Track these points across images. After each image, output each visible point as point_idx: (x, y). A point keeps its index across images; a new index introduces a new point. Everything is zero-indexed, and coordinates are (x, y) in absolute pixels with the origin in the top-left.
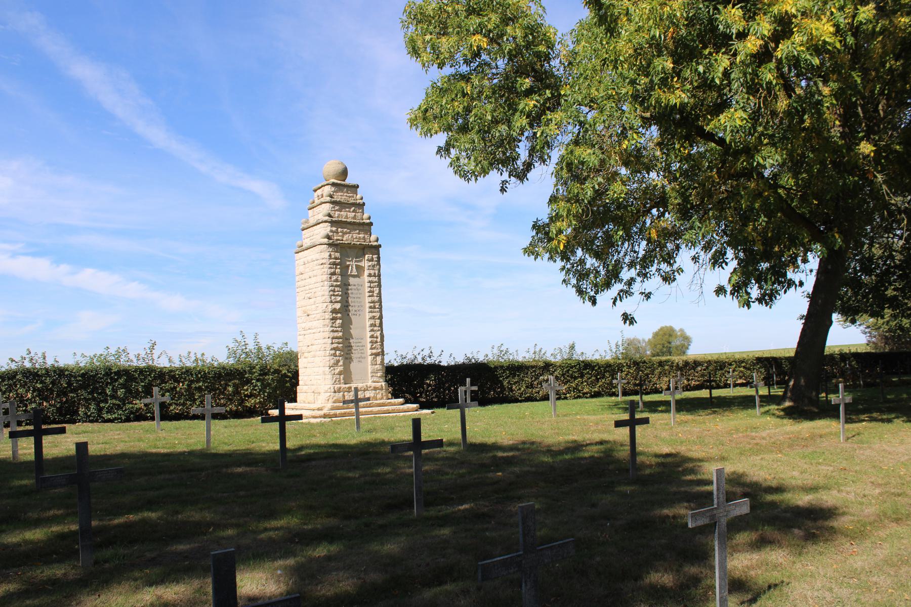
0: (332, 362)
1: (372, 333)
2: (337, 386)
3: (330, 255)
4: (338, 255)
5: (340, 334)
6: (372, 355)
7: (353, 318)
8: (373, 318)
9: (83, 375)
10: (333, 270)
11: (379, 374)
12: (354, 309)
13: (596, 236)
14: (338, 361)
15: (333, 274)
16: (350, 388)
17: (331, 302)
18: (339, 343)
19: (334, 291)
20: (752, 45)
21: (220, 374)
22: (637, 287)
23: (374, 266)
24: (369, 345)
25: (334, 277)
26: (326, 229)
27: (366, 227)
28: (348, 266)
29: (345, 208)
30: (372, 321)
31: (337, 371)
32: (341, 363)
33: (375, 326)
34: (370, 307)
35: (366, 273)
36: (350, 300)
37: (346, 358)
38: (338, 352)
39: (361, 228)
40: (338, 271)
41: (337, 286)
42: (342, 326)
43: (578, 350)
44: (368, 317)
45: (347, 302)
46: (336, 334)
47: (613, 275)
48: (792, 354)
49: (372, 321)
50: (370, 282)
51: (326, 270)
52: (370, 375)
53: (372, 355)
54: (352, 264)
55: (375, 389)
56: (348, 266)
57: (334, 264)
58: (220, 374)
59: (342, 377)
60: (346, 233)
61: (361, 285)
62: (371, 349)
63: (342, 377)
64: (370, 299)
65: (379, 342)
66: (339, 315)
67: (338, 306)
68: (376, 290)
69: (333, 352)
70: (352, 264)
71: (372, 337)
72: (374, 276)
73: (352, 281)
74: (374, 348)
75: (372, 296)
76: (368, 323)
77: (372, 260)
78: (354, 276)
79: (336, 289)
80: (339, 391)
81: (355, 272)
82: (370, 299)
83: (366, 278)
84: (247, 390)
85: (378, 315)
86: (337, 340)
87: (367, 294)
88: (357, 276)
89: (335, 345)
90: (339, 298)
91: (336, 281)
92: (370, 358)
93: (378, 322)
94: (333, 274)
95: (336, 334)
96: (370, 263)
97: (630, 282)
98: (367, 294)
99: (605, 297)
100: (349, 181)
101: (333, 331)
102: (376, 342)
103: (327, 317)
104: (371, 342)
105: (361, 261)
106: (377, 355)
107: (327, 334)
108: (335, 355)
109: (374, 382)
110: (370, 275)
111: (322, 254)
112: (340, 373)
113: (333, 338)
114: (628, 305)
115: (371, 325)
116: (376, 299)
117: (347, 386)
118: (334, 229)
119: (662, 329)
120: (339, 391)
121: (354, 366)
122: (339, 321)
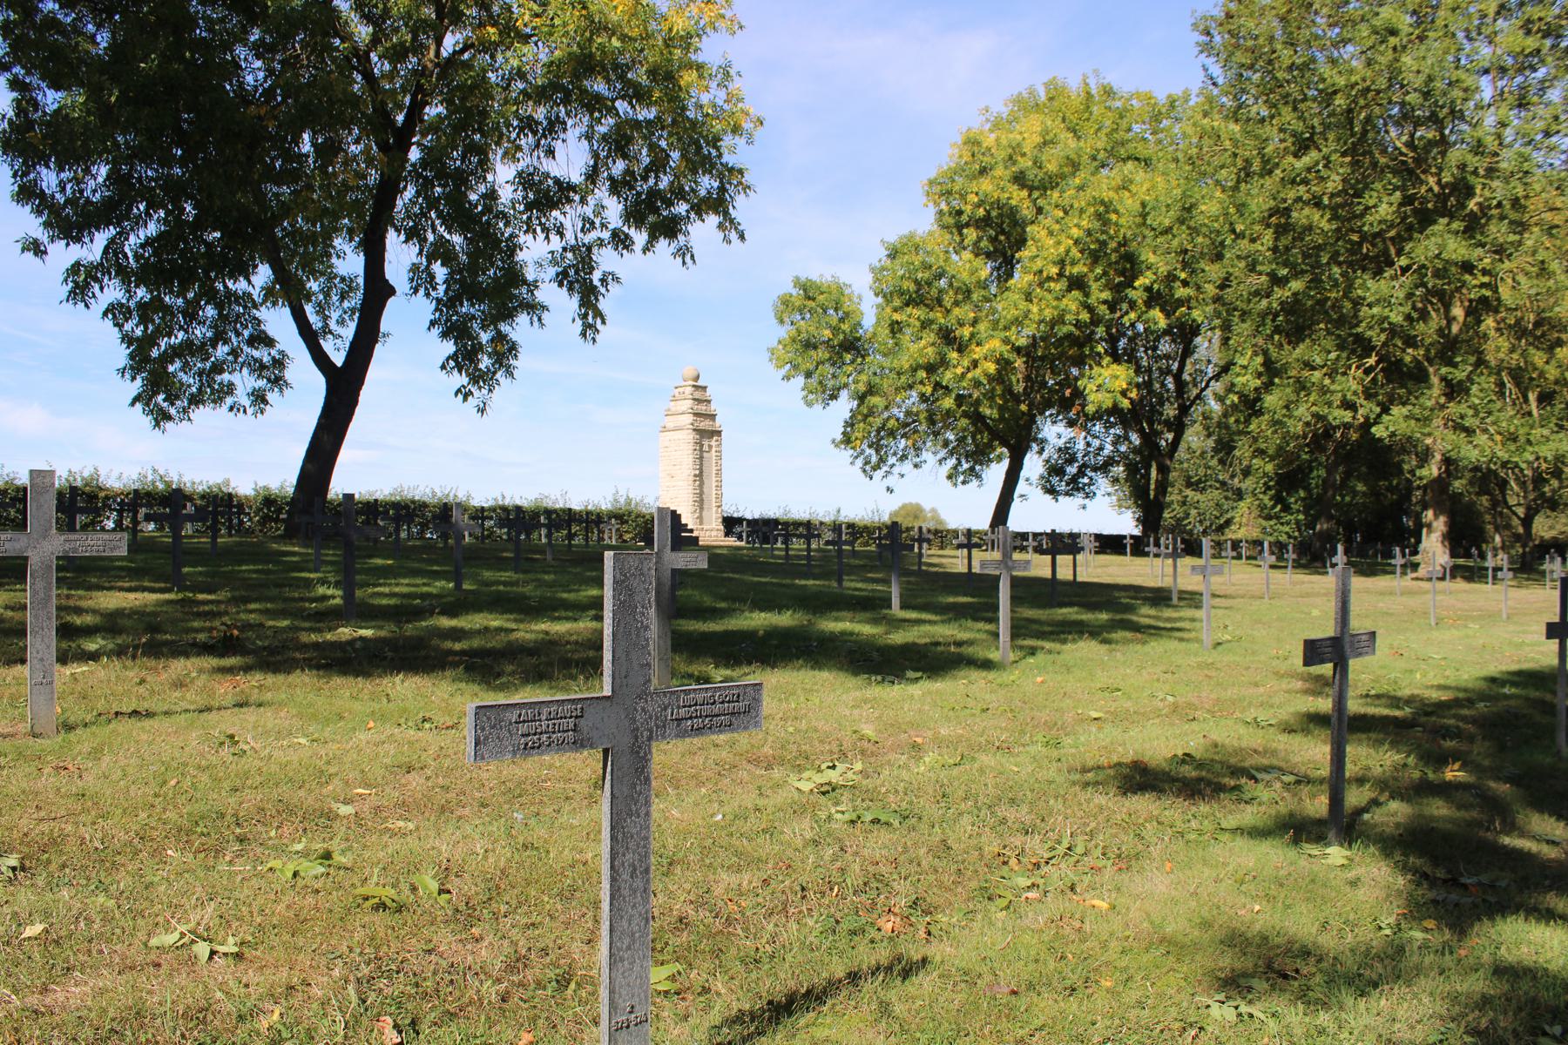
9: (203, 497)
13: (873, 438)
20: (959, 371)
22: (896, 470)
26: (690, 418)
27: (713, 417)
43: (843, 513)
47: (882, 460)
48: (290, 491)
51: (691, 447)
54: (706, 443)
65: (719, 497)
70: (706, 443)
97: (892, 466)
99: (878, 474)
100: (700, 383)
111: (688, 437)
114: (891, 481)
119: (904, 507)
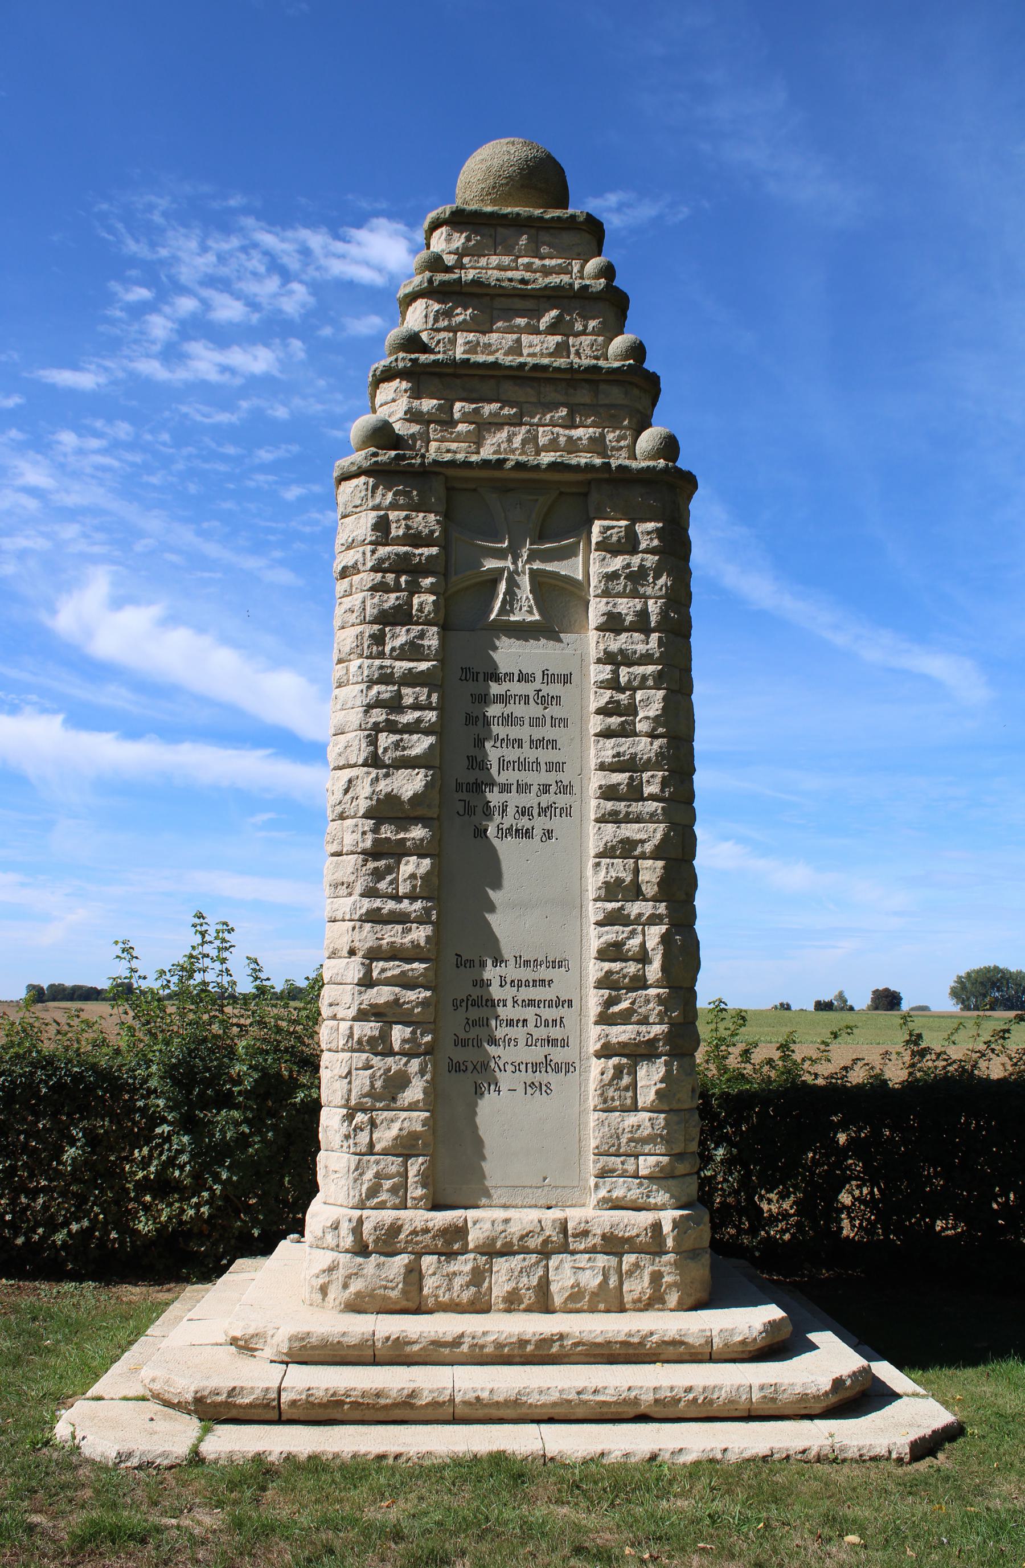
0: (362, 1081)
1: (612, 933)
2: (374, 1218)
3: (382, 526)
4: (426, 522)
5: (420, 934)
6: (606, 1052)
7: (507, 849)
8: (626, 849)
10: (391, 599)
11: (646, 1164)
12: (515, 800)
14: (398, 1083)
15: (388, 618)
16: (459, 1232)
17: (374, 761)
18: (405, 982)
19: (395, 705)
21: (31, 1087)
23: (637, 577)
24: (593, 1001)
25: (400, 637)
28: (493, 579)
29: (509, 314)
30: (619, 869)
31: (385, 1136)
32: (415, 1092)
33: (635, 892)
34: (609, 793)
35: (597, 610)
36: (493, 753)
37: (456, 1067)
38: (399, 1034)
39: (583, 396)
40: (424, 601)
41: (411, 679)
42: (430, 889)
44: (593, 845)
45: (478, 763)
46: (392, 935)
49: (619, 869)
50: (609, 658)
52: (591, 1166)
53: (606, 1052)
54: (515, 574)
55: (614, 1245)
56: (493, 579)
57: (401, 565)
58: (31, 1087)
59: (415, 1166)
60: (496, 424)
61: (566, 687)
62: (605, 1019)
63: (415, 1166)
64: (608, 749)
66: (417, 832)
67: (409, 784)
68: (651, 703)
69: (370, 1029)
70: (515, 574)
71: (612, 952)
72: (642, 624)
73: (508, 654)
74: (624, 1017)
75: (626, 731)
76: (593, 881)
77: (629, 545)
78: (523, 632)
79: (409, 695)
80: (388, 1242)
81: (526, 611)
82: (608, 749)
83: (593, 642)
84: (145, 1163)
85: (653, 833)
86: (394, 968)
87: (596, 724)
88: (547, 629)
89: (382, 995)
90: (420, 745)
91: (412, 651)
92: (596, 1071)
93: (651, 872)
94: (399, 616)
95: (392, 935)
96: (617, 563)
98: (596, 724)
101: (374, 917)
102: (639, 983)
103: (349, 840)
104: (605, 982)
105: (566, 554)
106: (638, 1053)
107: (342, 935)
108: (379, 1046)
109: (617, 1205)
110: (613, 624)
112: (405, 1148)
113: (374, 955)
115: (612, 890)
116: (645, 747)
117: (442, 1218)
118: (428, 404)
120: (388, 1242)
121: (499, 1113)
122: (411, 866)
